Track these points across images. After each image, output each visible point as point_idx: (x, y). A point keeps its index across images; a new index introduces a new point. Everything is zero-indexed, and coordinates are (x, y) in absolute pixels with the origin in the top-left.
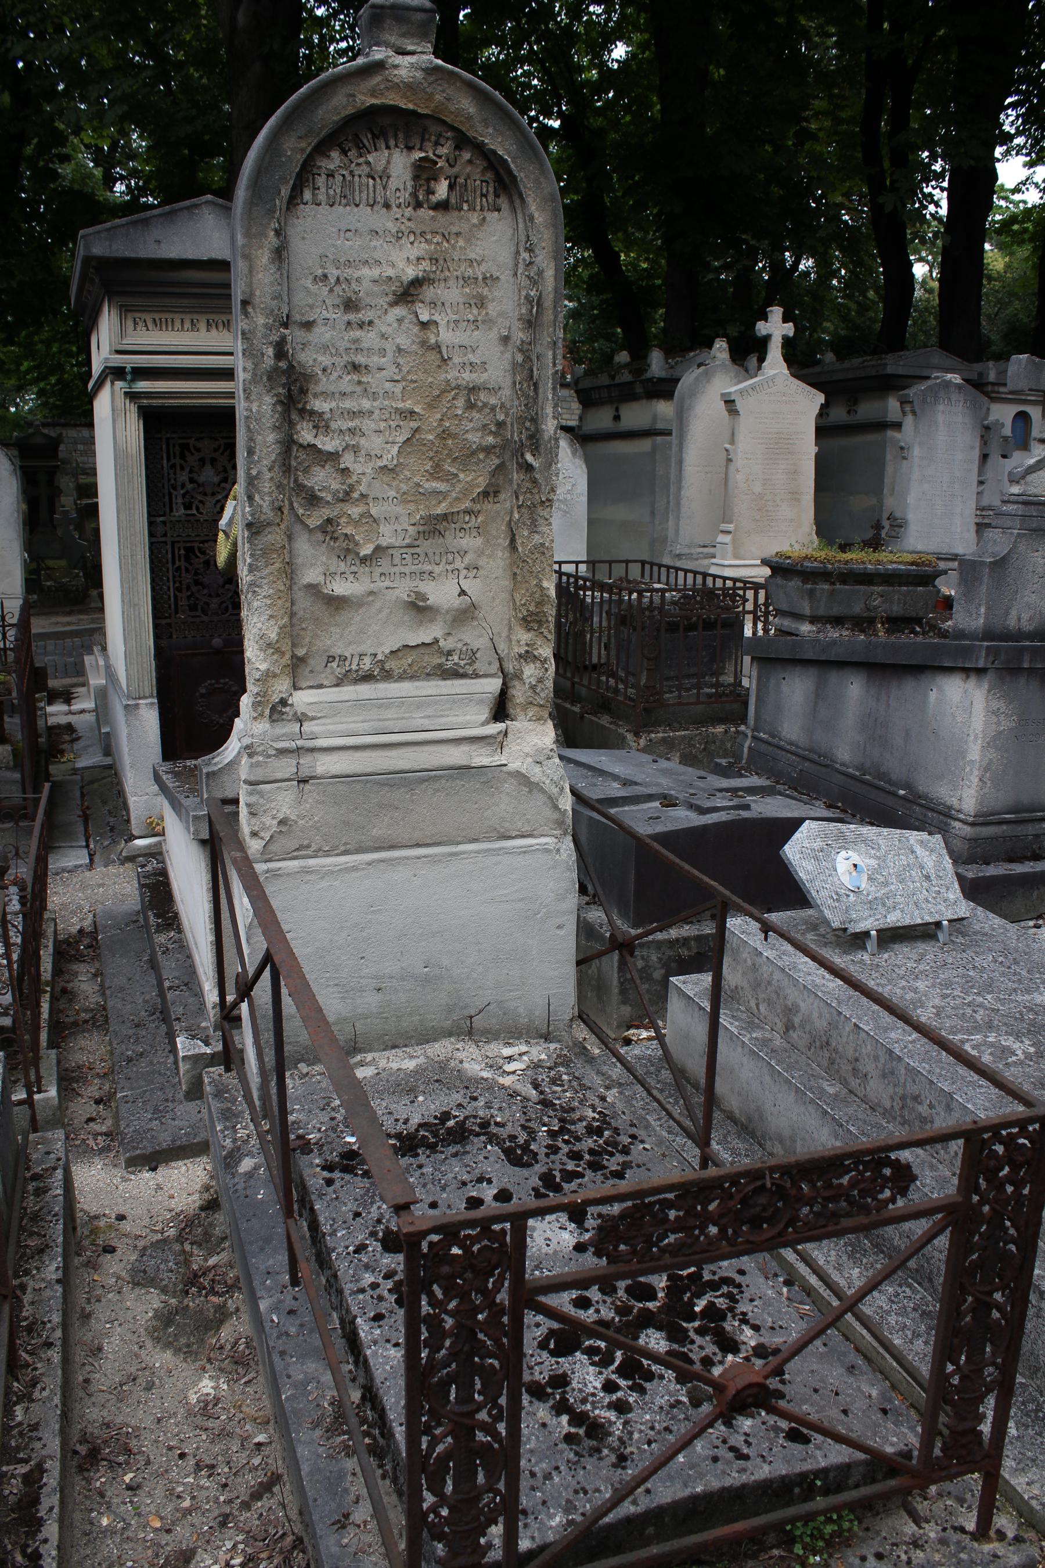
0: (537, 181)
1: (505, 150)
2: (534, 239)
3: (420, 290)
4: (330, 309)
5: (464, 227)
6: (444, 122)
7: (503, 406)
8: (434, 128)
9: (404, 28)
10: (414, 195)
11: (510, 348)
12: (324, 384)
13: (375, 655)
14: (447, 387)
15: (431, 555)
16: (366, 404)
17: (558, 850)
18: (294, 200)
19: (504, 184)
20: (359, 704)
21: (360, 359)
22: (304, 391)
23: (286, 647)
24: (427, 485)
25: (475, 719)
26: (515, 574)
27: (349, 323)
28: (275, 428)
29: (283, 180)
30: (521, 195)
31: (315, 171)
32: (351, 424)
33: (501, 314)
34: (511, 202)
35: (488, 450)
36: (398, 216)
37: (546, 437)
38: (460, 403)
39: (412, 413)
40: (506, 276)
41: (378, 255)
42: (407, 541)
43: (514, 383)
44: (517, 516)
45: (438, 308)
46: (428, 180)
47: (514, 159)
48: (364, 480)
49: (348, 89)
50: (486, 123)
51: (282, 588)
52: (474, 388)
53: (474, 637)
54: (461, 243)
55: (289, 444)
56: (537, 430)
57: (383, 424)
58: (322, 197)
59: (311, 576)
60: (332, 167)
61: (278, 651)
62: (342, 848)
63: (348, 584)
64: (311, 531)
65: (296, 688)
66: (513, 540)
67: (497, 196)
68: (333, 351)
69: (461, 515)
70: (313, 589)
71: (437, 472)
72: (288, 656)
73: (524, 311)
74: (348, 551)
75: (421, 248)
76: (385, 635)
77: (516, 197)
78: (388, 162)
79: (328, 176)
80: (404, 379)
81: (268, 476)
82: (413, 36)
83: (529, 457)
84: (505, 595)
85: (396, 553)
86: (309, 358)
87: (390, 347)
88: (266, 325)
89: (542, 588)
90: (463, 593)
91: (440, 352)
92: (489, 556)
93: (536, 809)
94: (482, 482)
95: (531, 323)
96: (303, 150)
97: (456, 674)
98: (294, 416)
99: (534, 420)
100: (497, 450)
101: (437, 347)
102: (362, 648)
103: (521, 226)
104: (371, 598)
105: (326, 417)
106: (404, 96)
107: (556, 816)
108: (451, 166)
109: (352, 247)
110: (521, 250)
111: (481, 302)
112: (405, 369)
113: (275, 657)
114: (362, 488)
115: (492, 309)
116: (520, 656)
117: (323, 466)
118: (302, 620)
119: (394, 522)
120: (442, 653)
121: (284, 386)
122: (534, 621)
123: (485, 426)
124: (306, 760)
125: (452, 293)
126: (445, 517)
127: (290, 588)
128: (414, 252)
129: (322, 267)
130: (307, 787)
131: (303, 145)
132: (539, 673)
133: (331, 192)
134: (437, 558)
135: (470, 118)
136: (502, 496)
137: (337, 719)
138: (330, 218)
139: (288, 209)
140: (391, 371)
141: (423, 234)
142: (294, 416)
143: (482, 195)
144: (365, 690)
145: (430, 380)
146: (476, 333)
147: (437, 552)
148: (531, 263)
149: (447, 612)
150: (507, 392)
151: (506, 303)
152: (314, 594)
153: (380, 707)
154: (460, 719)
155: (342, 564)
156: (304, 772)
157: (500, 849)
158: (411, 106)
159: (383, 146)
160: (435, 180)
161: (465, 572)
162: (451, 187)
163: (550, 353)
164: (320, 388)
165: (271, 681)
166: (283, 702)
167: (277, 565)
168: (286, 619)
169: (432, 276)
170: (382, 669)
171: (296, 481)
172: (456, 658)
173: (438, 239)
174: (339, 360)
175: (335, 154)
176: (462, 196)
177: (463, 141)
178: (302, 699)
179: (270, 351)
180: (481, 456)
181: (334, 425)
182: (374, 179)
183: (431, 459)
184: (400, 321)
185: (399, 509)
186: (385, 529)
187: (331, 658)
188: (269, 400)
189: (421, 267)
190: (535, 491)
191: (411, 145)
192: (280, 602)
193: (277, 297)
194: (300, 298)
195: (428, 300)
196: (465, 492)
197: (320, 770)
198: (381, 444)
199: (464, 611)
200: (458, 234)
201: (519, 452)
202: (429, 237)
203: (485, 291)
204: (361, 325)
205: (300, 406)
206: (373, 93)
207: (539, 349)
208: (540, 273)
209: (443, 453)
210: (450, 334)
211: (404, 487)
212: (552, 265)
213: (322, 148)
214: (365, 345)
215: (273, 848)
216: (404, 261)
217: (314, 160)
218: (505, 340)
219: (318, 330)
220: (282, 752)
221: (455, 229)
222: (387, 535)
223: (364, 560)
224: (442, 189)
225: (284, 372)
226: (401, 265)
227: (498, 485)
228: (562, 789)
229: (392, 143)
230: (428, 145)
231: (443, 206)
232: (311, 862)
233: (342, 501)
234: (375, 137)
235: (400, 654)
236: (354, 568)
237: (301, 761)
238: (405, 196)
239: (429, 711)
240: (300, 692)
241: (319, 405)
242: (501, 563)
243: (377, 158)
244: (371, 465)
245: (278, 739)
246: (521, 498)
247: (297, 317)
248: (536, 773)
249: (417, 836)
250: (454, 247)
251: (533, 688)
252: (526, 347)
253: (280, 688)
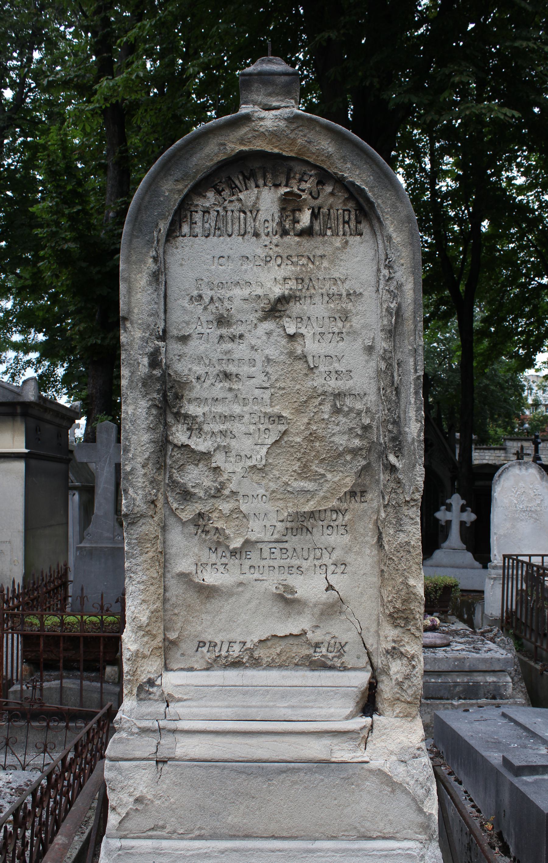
0: (394, 206)
1: (363, 181)
2: (393, 257)
3: (287, 306)
4: (205, 325)
5: (328, 250)
7: (368, 411)
8: (298, 168)
9: (270, 89)
10: (280, 224)
11: (374, 357)
12: (198, 391)
13: (244, 643)
14: (314, 394)
15: (299, 550)
16: (237, 409)
17: (423, 857)
18: (173, 233)
19: (363, 211)
20: (224, 690)
21: (232, 369)
22: (178, 397)
23: (158, 629)
24: (295, 484)
25: (340, 713)
26: (382, 571)
27: (221, 337)
28: (149, 429)
29: (162, 216)
30: (379, 219)
31: (193, 209)
32: (222, 427)
33: (364, 327)
34: (372, 227)
35: (355, 452)
36: (267, 243)
37: (410, 440)
38: (327, 408)
39: (280, 417)
40: (369, 293)
41: (247, 278)
42: (276, 536)
43: (379, 389)
44: (383, 515)
45: (304, 322)
46: (293, 211)
47: (371, 188)
48: (234, 478)
49: (221, 139)
50: (344, 159)
51: (155, 575)
52: (339, 394)
53: (342, 631)
54: (325, 264)
55: (163, 444)
56: (400, 433)
57: (253, 427)
58: (198, 229)
59: (183, 565)
60: (207, 205)
61: (148, 633)
62: (197, 833)
63: (219, 575)
64: (184, 524)
65: (167, 668)
66: (380, 538)
67: (358, 222)
68: (207, 362)
69: (328, 513)
70: (184, 577)
71: (304, 472)
72: (160, 638)
73: (385, 322)
74: (219, 544)
75: (288, 270)
76: (251, 623)
77: (375, 222)
78: (258, 198)
79: (204, 212)
80: (272, 386)
81: (143, 471)
82: (277, 95)
83: (392, 459)
84: (373, 592)
85: (266, 548)
86: (183, 368)
87: (259, 357)
88: (142, 339)
89: (408, 586)
90: (330, 587)
91: (307, 362)
92: (357, 553)
93: (399, 811)
94: (349, 481)
95: (393, 333)
96: (180, 191)
97: (323, 666)
98: (170, 419)
99: (396, 423)
100: (364, 452)
101: (304, 357)
102: (233, 636)
103: (381, 246)
104: (240, 589)
106: (270, 142)
107: (420, 819)
108: (314, 198)
109: (225, 271)
110: (382, 267)
111: (345, 316)
113: (145, 639)
114: (232, 486)
115: (356, 322)
116: (387, 652)
117: (197, 465)
118: (175, 606)
119: (263, 518)
120: (310, 644)
121: (158, 391)
122: (400, 618)
123: (351, 429)
124: (167, 740)
125: (318, 309)
126: (312, 515)
127: (164, 575)
128: (281, 273)
129: (198, 289)
130: (166, 767)
131: (180, 186)
132: (407, 670)
133: (207, 225)
134: (305, 554)
135: (329, 156)
136: (369, 496)
137: (202, 702)
138: (205, 247)
139: (167, 241)
140: (260, 379)
141: (289, 257)
142: (170, 419)
143: (344, 222)
144: (232, 676)
145: (298, 387)
146: (341, 344)
147: (306, 548)
148: (390, 279)
149: (315, 605)
150: (372, 398)
151: (369, 316)
152: (186, 583)
153: (245, 694)
154: (324, 712)
155: (214, 556)
156: (163, 753)
157: (359, 850)
158: (276, 151)
159: (253, 185)
160: (300, 210)
161: (333, 567)
162: (314, 216)
163: (411, 361)
165: (140, 662)
166: (151, 682)
167: (151, 554)
168: (158, 604)
169: (298, 294)
170: (251, 656)
171: (171, 477)
172: (324, 650)
173: (304, 261)
174: (212, 369)
175: (211, 194)
176: (325, 224)
177: (324, 177)
178: (171, 681)
179: (145, 361)
180: (348, 458)
181: (206, 428)
182: (245, 213)
184: (269, 334)
185: (269, 507)
186: (254, 524)
187: (201, 644)
188: (144, 404)
189: (287, 286)
190: (400, 491)
192: (152, 588)
193: (154, 314)
194: (176, 316)
195: (294, 315)
196: (332, 491)
197: (179, 752)
198: (250, 444)
199: (332, 606)
201: (383, 455)
202: (295, 259)
203: (350, 306)
204: (232, 339)
205: (175, 410)
206: (242, 141)
207: (399, 356)
208: (400, 286)
209: (314, 454)
210: (317, 344)
211: (273, 486)
212: (411, 279)
213: (198, 189)
214: (236, 356)
215: (128, 824)
216: (272, 282)
217: (192, 200)
218: (370, 349)
219: (193, 343)
220: (144, 731)
221: (319, 253)
222: (256, 530)
223: (234, 553)
224: (305, 218)
225: (158, 379)
226: (269, 284)
227: (364, 485)
228: (428, 791)
229: (261, 182)
231: (308, 232)
232: (165, 844)
233: (214, 497)
234: (246, 178)
235: (269, 643)
236: (224, 560)
237: (162, 742)
238: (273, 226)
239: (294, 701)
240: (171, 674)
241: (192, 409)
242: (370, 561)
243: (247, 196)
244: (241, 464)
245: (142, 718)
246: (387, 498)
247: (173, 332)
248: (400, 773)
249: (273, 827)
250: (319, 268)
251: (400, 684)
252: (388, 355)
253: (149, 669)
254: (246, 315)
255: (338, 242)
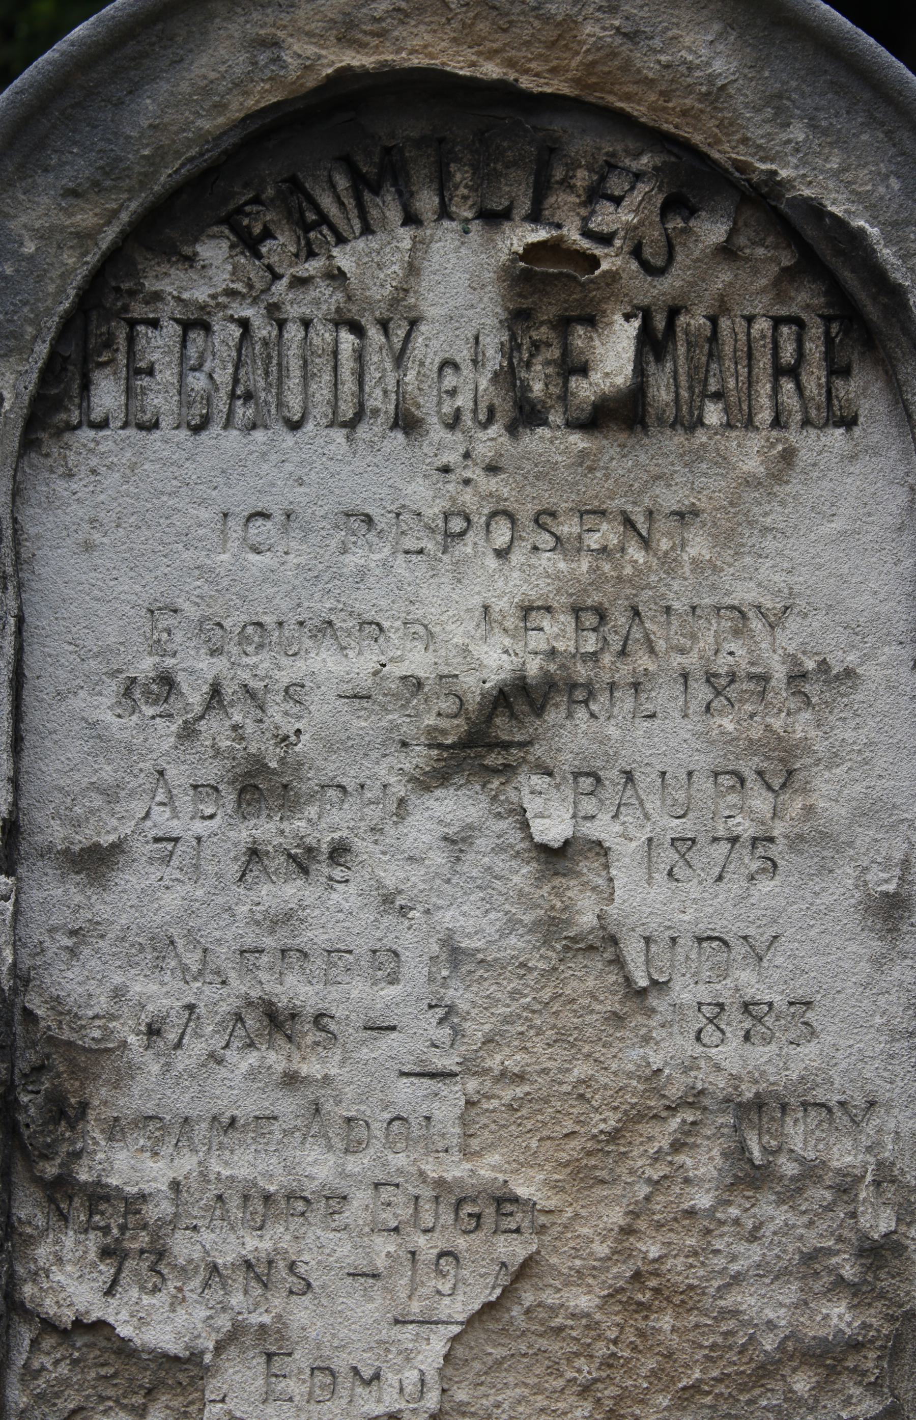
1: (858, 197)
3: (533, 725)
4: (185, 801)
5: (710, 489)
6: (624, 122)
7: (885, 1175)
8: (584, 144)
10: (509, 377)
12: (150, 1084)
14: (652, 1102)
16: (319, 1165)
21: (297, 990)
27: (254, 853)
31: (138, 310)
32: (255, 1244)
33: (867, 812)
36: (451, 458)
38: (706, 1162)
39: (504, 1200)
41: (366, 602)
45: (609, 792)
46: (564, 325)
47: (894, 229)
50: (778, 107)
52: (759, 1104)
54: (698, 546)
57: (384, 1247)
58: (160, 399)
60: (201, 294)
67: (838, 370)
68: (193, 960)
75: (539, 571)
78: (412, 269)
79: (187, 326)
87: (414, 943)
91: (619, 962)
96: (84, 237)
100: (869, 1360)
101: (606, 943)
105: (152, 1212)
109: (271, 578)
111: (784, 770)
112: (476, 1030)
115: (830, 793)
123: (811, 1257)
125: (665, 736)
128: (510, 585)
129: (157, 648)
131: (85, 218)
133: (198, 382)
135: (716, 95)
140: (418, 1038)
141: (543, 518)
143: (779, 371)
145: (581, 1070)
146: (766, 885)
158: (492, 70)
159: (394, 214)
160: (591, 321)
162: (652, 344)
164: (132, 1101)
169: (582, 672)
173: (607, 533)
175: (214, 252)
177: (693, 179)
180: (802, 1383)
181: (183, 1247)
182: (358, 330)
183: (585, 1390)
184: (457, 842)
189: (537, 641)
191: (497, 204)
195: (566, 761)
200: (684, 516)
202: (568, 527)
203: (802, 725)
204: (302, 862)
205: (51, 1170)
210: (661, 888)
213: (164, 226)
214: (315, 936)
216: (471, 622)
217: (134, 274)
219: (131, 880)
221: (670, 498)
224: (613, 353)
229: (427, 202)
230: (563, 202)
231: (623, 414)
238: (476, 385)
241: (124, 1165)
243: (371, 260)
247: (54, 832)
250: (669, 563)
254: (360, 763)
255: (750, 454)
